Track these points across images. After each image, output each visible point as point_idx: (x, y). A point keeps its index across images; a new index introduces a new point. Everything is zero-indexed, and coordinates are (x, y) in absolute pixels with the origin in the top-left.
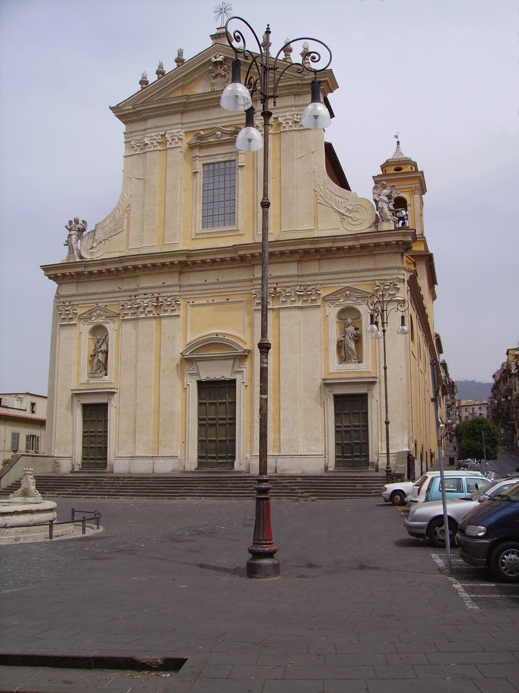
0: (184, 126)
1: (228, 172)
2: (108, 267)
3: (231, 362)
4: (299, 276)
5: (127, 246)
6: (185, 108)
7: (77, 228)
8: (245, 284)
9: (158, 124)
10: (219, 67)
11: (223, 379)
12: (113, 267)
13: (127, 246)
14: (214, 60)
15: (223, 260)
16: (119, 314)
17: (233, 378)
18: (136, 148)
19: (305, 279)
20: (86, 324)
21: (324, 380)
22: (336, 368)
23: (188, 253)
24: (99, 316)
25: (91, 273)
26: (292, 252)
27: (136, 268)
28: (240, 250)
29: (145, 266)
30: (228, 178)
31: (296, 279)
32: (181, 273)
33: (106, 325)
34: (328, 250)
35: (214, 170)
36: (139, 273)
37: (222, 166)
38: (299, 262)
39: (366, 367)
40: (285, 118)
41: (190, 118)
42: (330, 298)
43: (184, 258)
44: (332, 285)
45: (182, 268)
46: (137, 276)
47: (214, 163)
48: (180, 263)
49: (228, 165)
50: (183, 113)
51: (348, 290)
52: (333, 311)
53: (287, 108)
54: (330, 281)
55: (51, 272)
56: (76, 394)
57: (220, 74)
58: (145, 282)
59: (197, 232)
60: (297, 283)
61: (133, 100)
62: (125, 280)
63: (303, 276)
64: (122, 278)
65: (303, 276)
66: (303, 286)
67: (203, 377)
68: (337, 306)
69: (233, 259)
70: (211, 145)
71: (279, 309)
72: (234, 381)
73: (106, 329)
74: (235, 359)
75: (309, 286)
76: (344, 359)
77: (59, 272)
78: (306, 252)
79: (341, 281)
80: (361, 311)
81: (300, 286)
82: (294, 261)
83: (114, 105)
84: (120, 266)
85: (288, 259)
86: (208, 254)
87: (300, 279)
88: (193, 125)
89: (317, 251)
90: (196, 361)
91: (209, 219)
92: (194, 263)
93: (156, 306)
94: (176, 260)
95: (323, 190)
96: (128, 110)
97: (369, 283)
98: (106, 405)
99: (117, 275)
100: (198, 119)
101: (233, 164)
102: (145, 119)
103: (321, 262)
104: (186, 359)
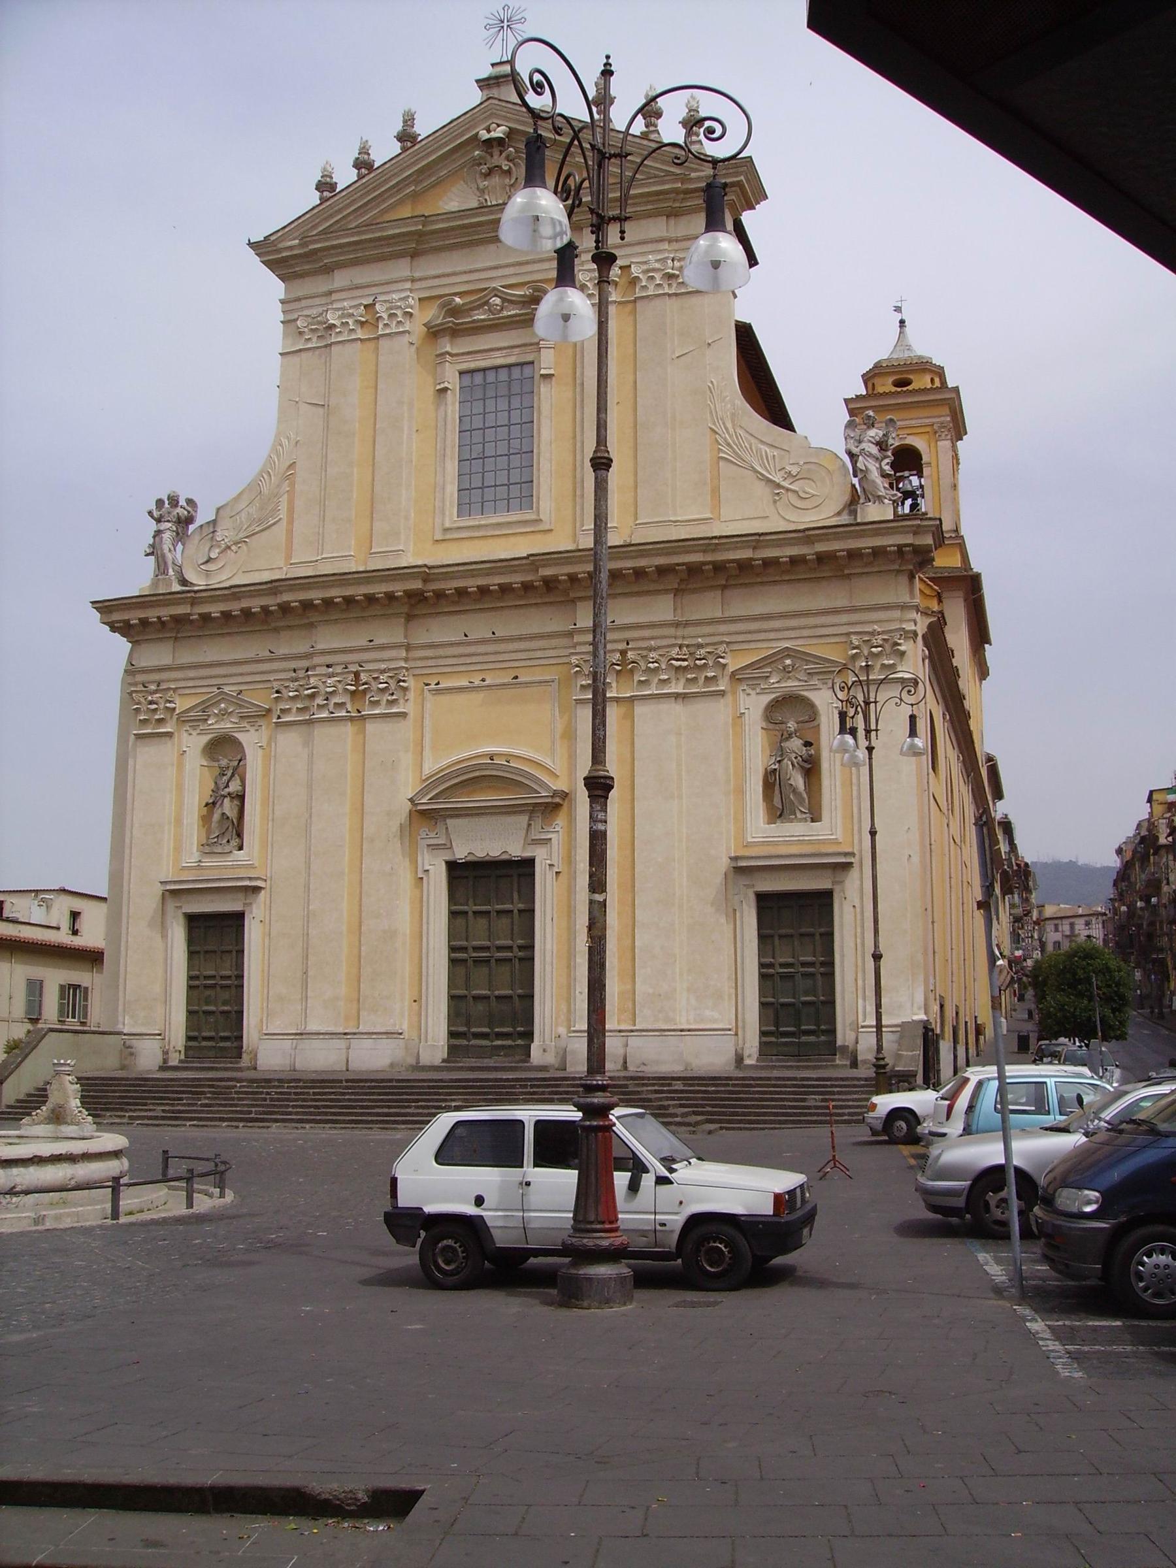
0: (418, 285)
1: (516, 388)
2: (245, 604)
3: (524, 819)
4: (677, 625)
5: (289, 556)
6: (419, 243)
7: (175, 516)
8: (554, 642)
9: (359, 281)
10: (496, 152)
11: (505, 857)
12: (255, 604)
13: (289, 556)
14: (484, 135)
15: (505, 589)
16: (269, 711)
17: (527, 854)
18: (309, 336)
19: (690, 631)
20: (194, 733)
21: (735, 859)
22: (761, 833)
23: (426, 573)
24: (224, 714)
25: (206, 618)
26: (662, 571)
27: (307, 605)
28: (544, 566)
29: (328, 603)
30: (516, 402)
31: (672, 631)
32: (410, 617)
33: (240, 736)
34: (744, 566)
35: (485, 385)
36: (314, 617)
37: (503, 375)
38: (677, 592)
39: (830, 831)
40: (645, 267)
41: (430, 266)
42: (748, 673)
43: (417, 585)
44: (753, 645)
45: (412, 606)
46: (311, 625)
47: (484, 370)
48: (409, 594)
49: (516, 372)
50: (414, 255)
51: (788, 656)
52: (754, 704)
53: (650, 245)
54: (749, 637)
55: (116, 616)
56: (172, 892)
57: (500, 167)
58: (329, 638)
59: (447, 525)
60: (673, 641)
61: (302, 225)
62: (283, 633)
63: (687, 624)
64: (276, 630)
65: (687, 624)
66: (688, 646)
67: (461, 853)
68: (763, 692)
69: (527, 587)
70: (478, 329)
71: (632, 699)
72: (530, 863)
73: (240, 743)
74: (532, 812)
75: (700, 646)
76: (778, 812)
77: (134, 617)
78: (693, 570)
79: (772, 635)
80: (817, 702)
81: (681, 647)
82: (666, 591)
83: (258, 237)
84: (271, 602)
85: (652, 587)
86: (472, 574)
87: (680, 632)
88: (437, 282)
89: (719, 568)
90: (445, 817)
91: (473, 496)
92: (440, 595)
93: (353, 693)
94: (398, 588)
95: (731, 430)
96: (291, 248)
97: (837, 639)
98: (239, 917)
99: (264, 622)
100: (449, 270)
101: (527, 371)
102: (328, 270)
103: (728, 593)
104: (423, 813)
